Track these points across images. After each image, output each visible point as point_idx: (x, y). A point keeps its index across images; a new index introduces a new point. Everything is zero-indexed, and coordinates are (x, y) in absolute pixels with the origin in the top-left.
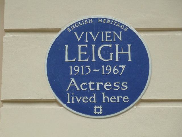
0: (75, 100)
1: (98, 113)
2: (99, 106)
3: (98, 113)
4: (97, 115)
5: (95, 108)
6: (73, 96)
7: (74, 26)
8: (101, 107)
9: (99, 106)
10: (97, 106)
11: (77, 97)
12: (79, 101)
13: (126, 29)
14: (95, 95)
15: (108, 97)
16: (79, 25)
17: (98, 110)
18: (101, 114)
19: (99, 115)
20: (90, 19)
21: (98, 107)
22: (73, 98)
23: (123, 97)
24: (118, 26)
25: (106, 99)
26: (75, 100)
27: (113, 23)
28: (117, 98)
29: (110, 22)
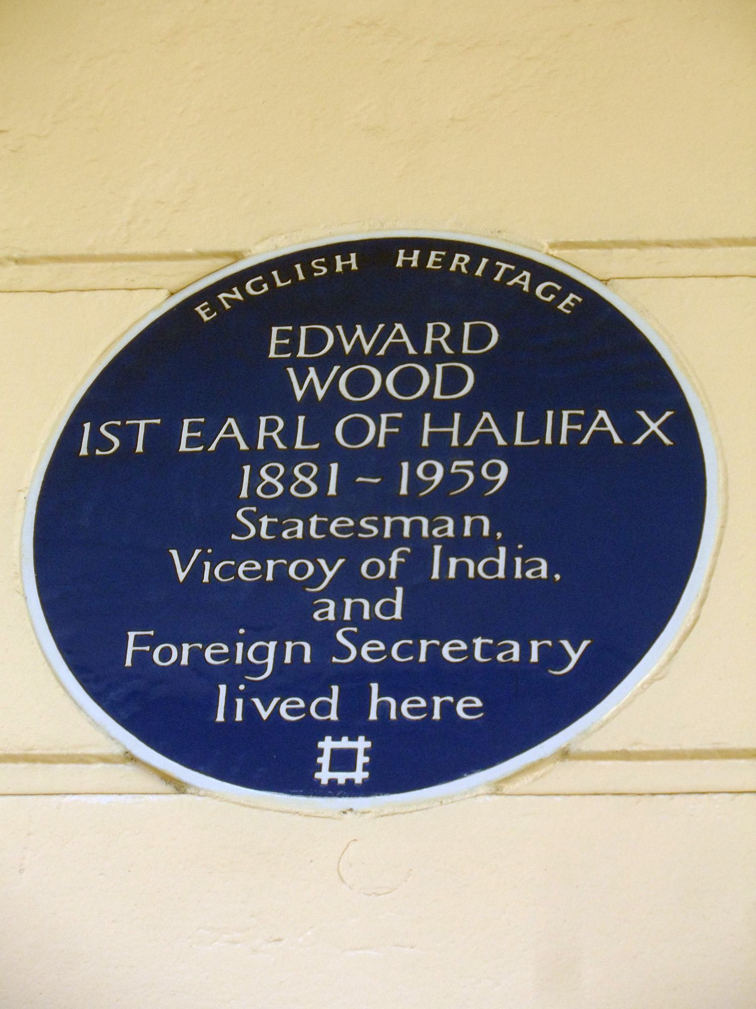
0: (250, 710)
1: (342, 777)
2: (365, 768)
3: (342, 777)
4: (333, 789)
5: (327, 744)
6: (240, 694)
7: (243, 291)
8: (362, 744)
9: (321, 752)
10: (336, 738)
11: (257, 701)
12: (265, 715)
13: (568, 301)
14: (335, 689)
15: (392, 702)
16: (272, 283)
17: (343, 760)
18: (358, 781)
19: (350, 789)
20: (344, 249)
21: (345, 739)
22: (240, 702)
23: (456, 700)
24: (519, 287)
25: (383, 709)
26: (250, 710)
27: (491, 270)
28: (431, 704)
29: (473, 266)
